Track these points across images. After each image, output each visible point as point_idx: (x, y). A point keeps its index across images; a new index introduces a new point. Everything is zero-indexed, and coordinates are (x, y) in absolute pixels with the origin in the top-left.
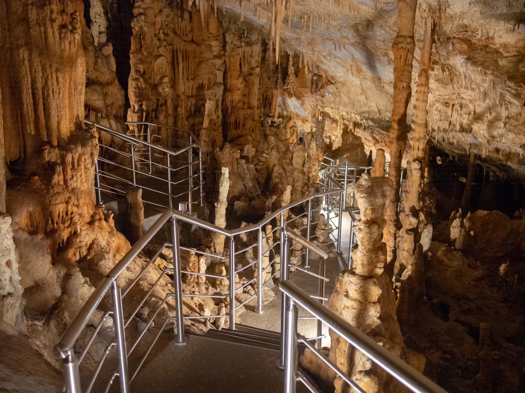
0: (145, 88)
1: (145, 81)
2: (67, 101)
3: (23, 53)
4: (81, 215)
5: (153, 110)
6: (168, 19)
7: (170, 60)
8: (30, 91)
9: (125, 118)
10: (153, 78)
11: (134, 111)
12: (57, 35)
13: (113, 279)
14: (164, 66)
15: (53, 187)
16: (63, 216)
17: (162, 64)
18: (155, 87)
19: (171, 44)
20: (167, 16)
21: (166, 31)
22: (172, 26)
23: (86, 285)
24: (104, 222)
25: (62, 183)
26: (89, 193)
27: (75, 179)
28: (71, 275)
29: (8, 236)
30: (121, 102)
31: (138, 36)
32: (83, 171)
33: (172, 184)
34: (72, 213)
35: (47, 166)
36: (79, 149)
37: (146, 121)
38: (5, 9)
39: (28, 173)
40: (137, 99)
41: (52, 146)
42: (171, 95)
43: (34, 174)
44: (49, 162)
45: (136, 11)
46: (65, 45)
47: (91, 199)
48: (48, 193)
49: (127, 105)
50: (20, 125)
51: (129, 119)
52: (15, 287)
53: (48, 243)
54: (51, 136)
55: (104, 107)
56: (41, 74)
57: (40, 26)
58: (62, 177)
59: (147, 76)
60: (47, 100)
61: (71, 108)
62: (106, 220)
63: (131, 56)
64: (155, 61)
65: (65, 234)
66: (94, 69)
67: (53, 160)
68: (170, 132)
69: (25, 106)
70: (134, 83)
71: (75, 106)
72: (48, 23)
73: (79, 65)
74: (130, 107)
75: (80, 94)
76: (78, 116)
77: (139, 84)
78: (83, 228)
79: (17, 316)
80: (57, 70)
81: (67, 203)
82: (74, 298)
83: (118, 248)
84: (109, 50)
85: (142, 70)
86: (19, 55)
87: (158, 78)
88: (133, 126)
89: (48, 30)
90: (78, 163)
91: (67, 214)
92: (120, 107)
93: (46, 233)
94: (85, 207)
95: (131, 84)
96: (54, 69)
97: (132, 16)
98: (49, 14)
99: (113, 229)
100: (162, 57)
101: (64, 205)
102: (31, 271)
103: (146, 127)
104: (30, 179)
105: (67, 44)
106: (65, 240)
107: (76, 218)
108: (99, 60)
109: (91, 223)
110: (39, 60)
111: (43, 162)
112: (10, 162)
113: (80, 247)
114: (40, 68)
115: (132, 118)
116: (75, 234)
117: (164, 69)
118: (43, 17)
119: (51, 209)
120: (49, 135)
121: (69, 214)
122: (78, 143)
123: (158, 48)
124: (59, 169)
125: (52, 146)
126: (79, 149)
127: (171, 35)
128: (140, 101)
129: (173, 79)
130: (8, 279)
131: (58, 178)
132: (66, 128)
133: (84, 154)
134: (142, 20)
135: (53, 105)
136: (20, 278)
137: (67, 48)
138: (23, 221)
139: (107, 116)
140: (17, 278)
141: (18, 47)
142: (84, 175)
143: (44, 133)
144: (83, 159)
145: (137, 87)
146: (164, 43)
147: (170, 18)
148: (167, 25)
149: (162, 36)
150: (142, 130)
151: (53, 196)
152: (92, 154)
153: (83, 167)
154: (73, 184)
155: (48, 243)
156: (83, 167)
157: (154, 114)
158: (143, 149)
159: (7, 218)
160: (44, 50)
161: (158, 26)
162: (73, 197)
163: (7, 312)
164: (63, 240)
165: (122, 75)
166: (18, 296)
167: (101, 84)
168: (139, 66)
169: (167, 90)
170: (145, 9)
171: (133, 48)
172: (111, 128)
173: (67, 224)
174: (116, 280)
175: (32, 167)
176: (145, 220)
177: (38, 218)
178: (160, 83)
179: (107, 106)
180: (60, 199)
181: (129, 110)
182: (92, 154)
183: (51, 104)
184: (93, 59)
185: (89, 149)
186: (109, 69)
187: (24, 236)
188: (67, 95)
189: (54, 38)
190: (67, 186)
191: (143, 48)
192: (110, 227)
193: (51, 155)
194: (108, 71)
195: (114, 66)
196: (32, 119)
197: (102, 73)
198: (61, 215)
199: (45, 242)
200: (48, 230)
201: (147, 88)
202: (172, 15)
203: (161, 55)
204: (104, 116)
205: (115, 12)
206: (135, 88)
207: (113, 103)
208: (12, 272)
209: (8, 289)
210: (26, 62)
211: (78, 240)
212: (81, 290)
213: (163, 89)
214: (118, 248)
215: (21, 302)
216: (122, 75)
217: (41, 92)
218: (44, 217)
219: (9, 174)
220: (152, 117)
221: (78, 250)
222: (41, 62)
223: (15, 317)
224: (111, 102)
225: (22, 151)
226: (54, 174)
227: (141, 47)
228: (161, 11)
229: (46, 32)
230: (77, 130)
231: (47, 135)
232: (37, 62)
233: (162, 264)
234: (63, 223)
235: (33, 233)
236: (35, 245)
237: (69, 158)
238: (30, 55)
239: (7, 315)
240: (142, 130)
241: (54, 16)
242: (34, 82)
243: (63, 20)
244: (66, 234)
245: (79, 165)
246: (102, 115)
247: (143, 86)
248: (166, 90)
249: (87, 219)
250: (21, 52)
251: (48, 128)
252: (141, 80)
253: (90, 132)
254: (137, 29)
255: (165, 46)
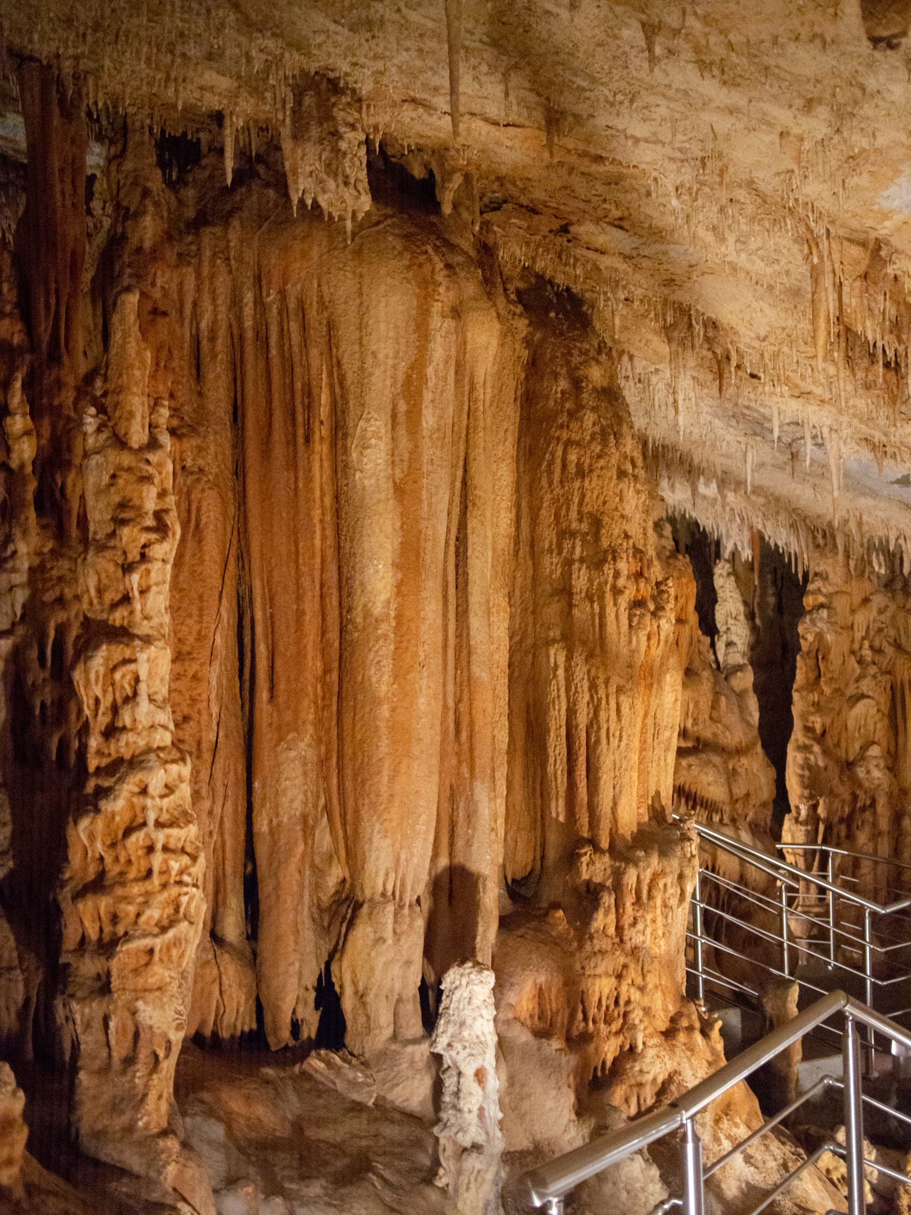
0: (826, 768)
1: (825, 752)
2: (635, 758)
3: (557, 655)
4: (647, 1011)
5: (841, 820)
6: (882, 618)
7: (885, 709)
8: (563, 731)
9: (778, 838)
10: (843, 745)
11: (797, 820)
12: (624, 620)
13: (686, 1115)
14: (870, 722)
15: (591, 938)
16: (608, 1007)
17: (866, 715)
18: (848, 766)
19: (889, 673)
20: (881, 612)
21: (877, 644)
22: (892, 632)
23: (639, 1158)
24: (698, 1037)
25: (612, 931)
26: (670, 965)
27: (640, 926)
28: (607, 1128)
29: (484, 1012)
30: (766, 792)
31: (813, 654)
32: (659, 911)
33: (873, 984)
34: (628, 1002)
35: (583, 889)
36: (655, 860)
37: (825, 842)
38: (530, 572)
39: (545, 905)
40: (806, 793)
41: (597, 849)
42: (885, 786)
43: (556, 906)
44: (588, 883)
45: (809, 601)
46: (638, 642)
47: (673, 978)
48: (580, 947)
49: (781, 804)
50: (539, 802)
51: (786, 836)
52: (487, 1133)
53: (570, 1061)
54: (598, 826)
55: (727, 800)
56: (587, 697)
57: (592, 602)
58: (612, 917)
59: (829, 741)
60: (595, 750)
61: (643, 773)
62: (705, 1033)
63: (796, 696)
64: (851, 707)
65: (610, 1049)
66: (711, 718)
67: (597, 879)
68: (882, 869)
69: (551, 760)
70: (800, 757)
71: (654, 772)
72: (609, 597)
73: (667, 688)
74: (789, 811)
75: (667, 750)
76: (658, 793)
77: (812, 757)
78: (651, 1042)
79: (487, 1205)
80: (620, 690)
81: (619, 977)
82: (610, 1185)
83: (729, 1106)
84: (746, 680)
85: (818, 727)
86: (548, 657)
87: (857, 746)
88: (795, 854)
89: (608, 610)
90: (650, 891)
91: (617, 1002)
92: (764, 805)
93: (568, 1040)
94: (659, 995)
95: (794, 759)
96: (613, 689)
97: (800, 612)
98: (610, 579)
99: (718, 1056)
100: (866, 701)
101: (613, 981)
102: (528, 1118)
103: (825, 855)
104: (546, 914)
105: (644, 639)
106: (609, 1064)
107: (636, 1016)
108: (723, 699)
109: (669, 1034)
110: (585, 669)
111: (578, 881)
112: (514, 880)
113: (640, 1085)
114: (586, 684)
115: (792, 834)
116: (630, 1053)
117: (871, 727)
118: (599, 584)
119: (583, 986)
120: (594, 823)
121: (622, 1002)
122: (652, 848)
123: (857, 680)
124: (608, 899)
125: (597, 849)
126: (655, 860)
127: (890, 651)
128: (811, 797)
129: (892, 750)
130: (475, 1109)
131: (603, 920)
132: (630, 814)
133: (663, 873)
134: (821, 619)
135: (607, 760)
136: (500, 1115)
137: (643, 648)
138: (524, 1003)
139: (733, 820)
140: (494, 1113)
141: (548, 643)
142: (663, 922)
143: (584, 819)
144: (661, 885)
145: (807, 765)
146: (873, 670)
147: (888, 614)
148: (880, 630)
149: (867, 653)
150: (816, 864)
151: (588, 958)
152: (681, 877)
153: (659, 902)
154: (635, 937)
155: (570, 1061)
156: (659, 902)
157: (843, 828)
158: (816, 910)
159: (486, 972)
160: (596, 648)
161: (859, 635)
162: (632, 966)
163: (468, 1189)
164: (604, 1063)
165: (774, 735)
166: (492, 1156)
167: (723, 749)
168: (812, 718)
169: (876, 773)
170: (829, 596)
171: (800, 677)
172: (738, 840)
173: (615, 1027)
174: (692, 1118)
175: (553, 890)
176: (806, 1065)
177: (555, 1002)
178: (862, 756)
179: (734, 801)
180: (605, 965)
181: (787, 817)
182: (681, 877)
183: (602, 759)
184: (710, 696)
185: (675, 863)
186: (744, 720)
187: (522, 1036)
188: (636, 744)
189: (618, 627)
190: (622, 941)
191: (823, 679)
192: (713, 1051)
193: (594, 868)
194: (740, 723)
195: (756, 715)
196: (562, 787)
197: (727, 727)
198: (604, 1003)
199: (564, 1059)
200: (575, 1033)
201: (830, 768)
202: (893, 607)
203: (863, 696)
204: (726, 820)
205: (771, 613)
206: (803, 768)
207: (748, 795)
208: (485, 1096)
209: (473, 1134)
210: (561, 672)
211: (637, 1068)
212: (626, 1169)
213: (868, 772)
214: (729, 1106)
215: (498, 1173)
216: (774, 735)
217: (583, 734)
218: (569, 1001)
219: (509, 902)
220: (838, 836)
221: (635, 1090)
222: (589, 671)
223: (481, 1205)
224: (744, 791)
225: (538, 857)
226: (596, 908)
227: (819, 676)
228: (866, 601)
229: (602, 615)
230: (654, 823)
231: (590, 824)
232: (580, 671)
233: (836, 1168)
234: (608, 1022)
235: (542, 1034)
236: (544, 1062)
237: (631, 877)
238: (569, 658)
239: (466, 1195)
240: (816, 864)
241: (621, 582)
242: (571, 712)
243: (638, 590)
244: (612, 1049)
245: (650, 897)
246: (721, 820)
247: (821, 763)
248: (874, 773)
249: (662, 1024)
250: (552, 652)
251: (592, 808)
252: (816, 748)
253: (680, 829)
254: (810, 638)
255: (874, 677)
